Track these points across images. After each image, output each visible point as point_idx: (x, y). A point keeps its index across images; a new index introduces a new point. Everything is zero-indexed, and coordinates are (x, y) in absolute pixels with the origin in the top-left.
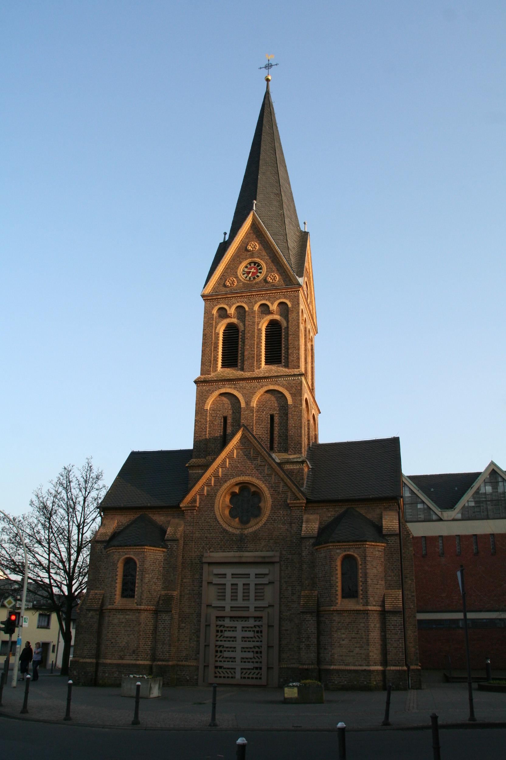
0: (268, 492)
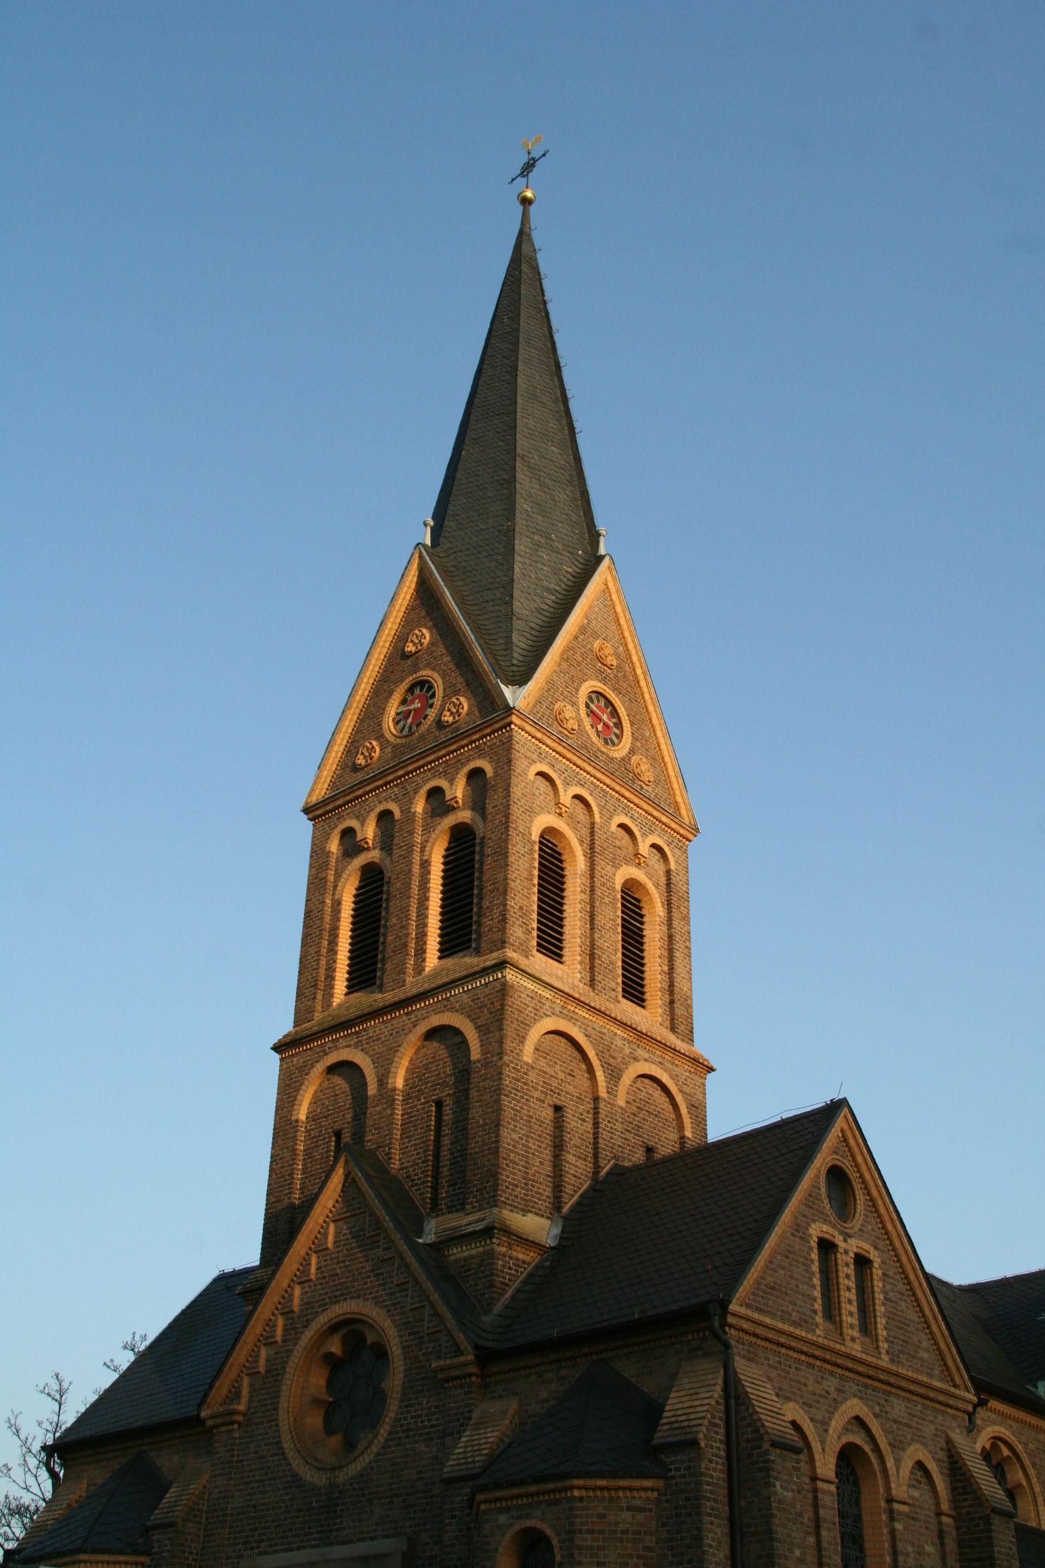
0: (397, 1340)
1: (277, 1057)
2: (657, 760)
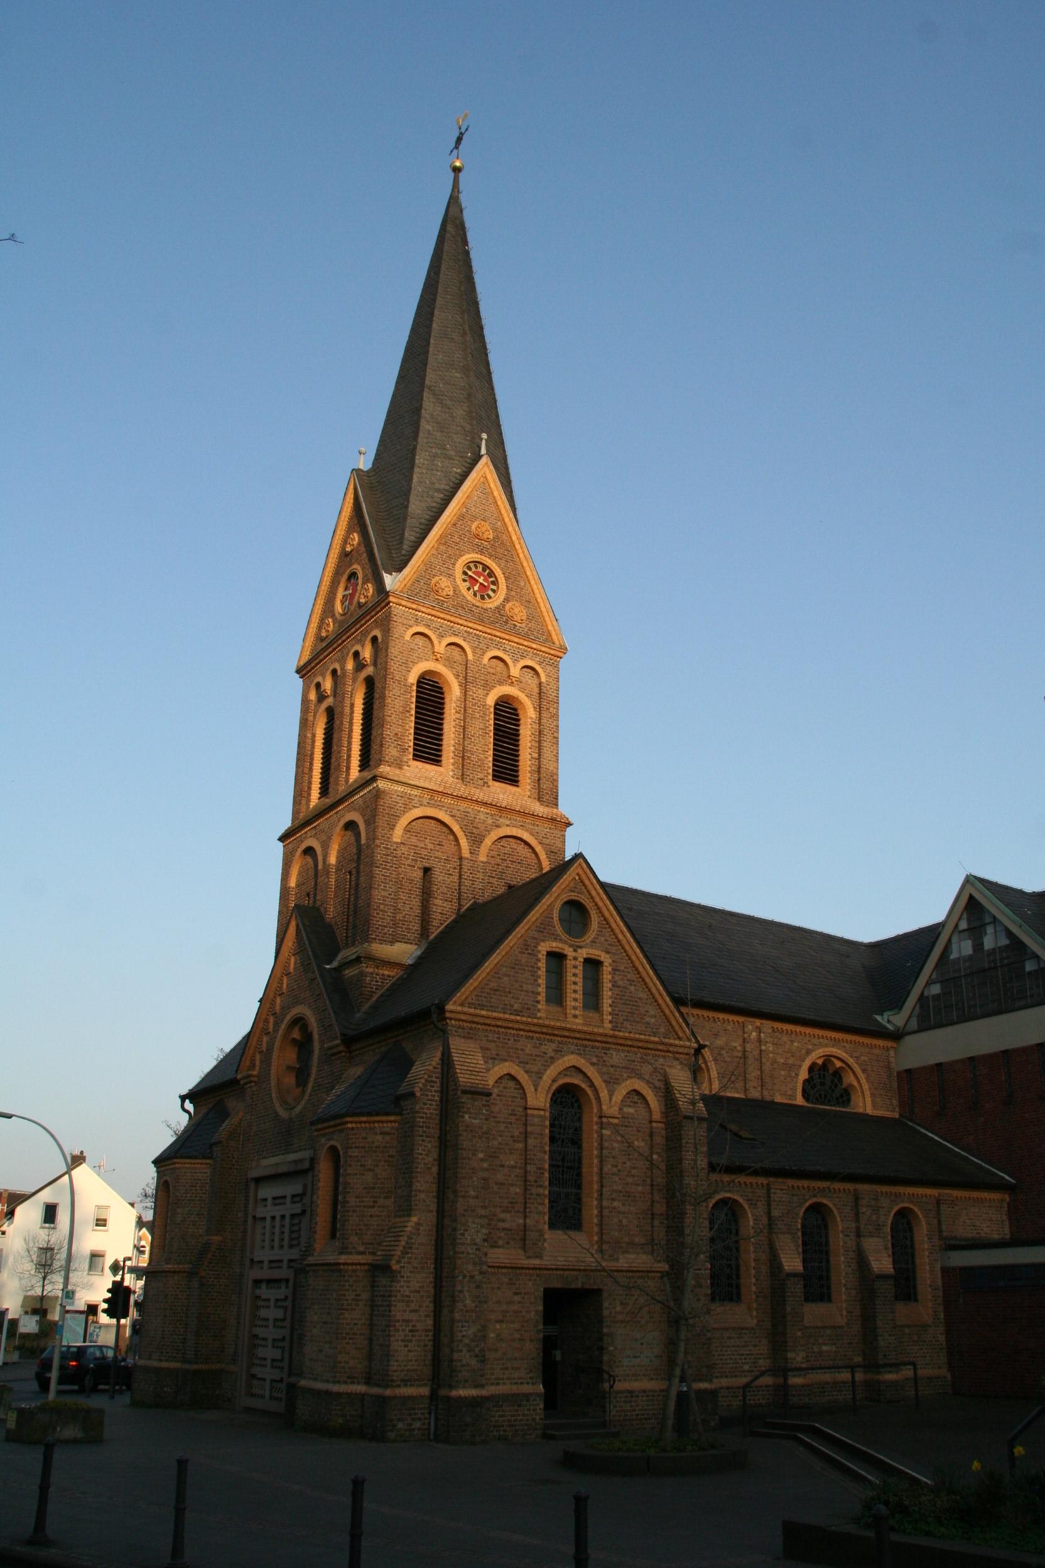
1: (281, 844)
2: (530, 603)
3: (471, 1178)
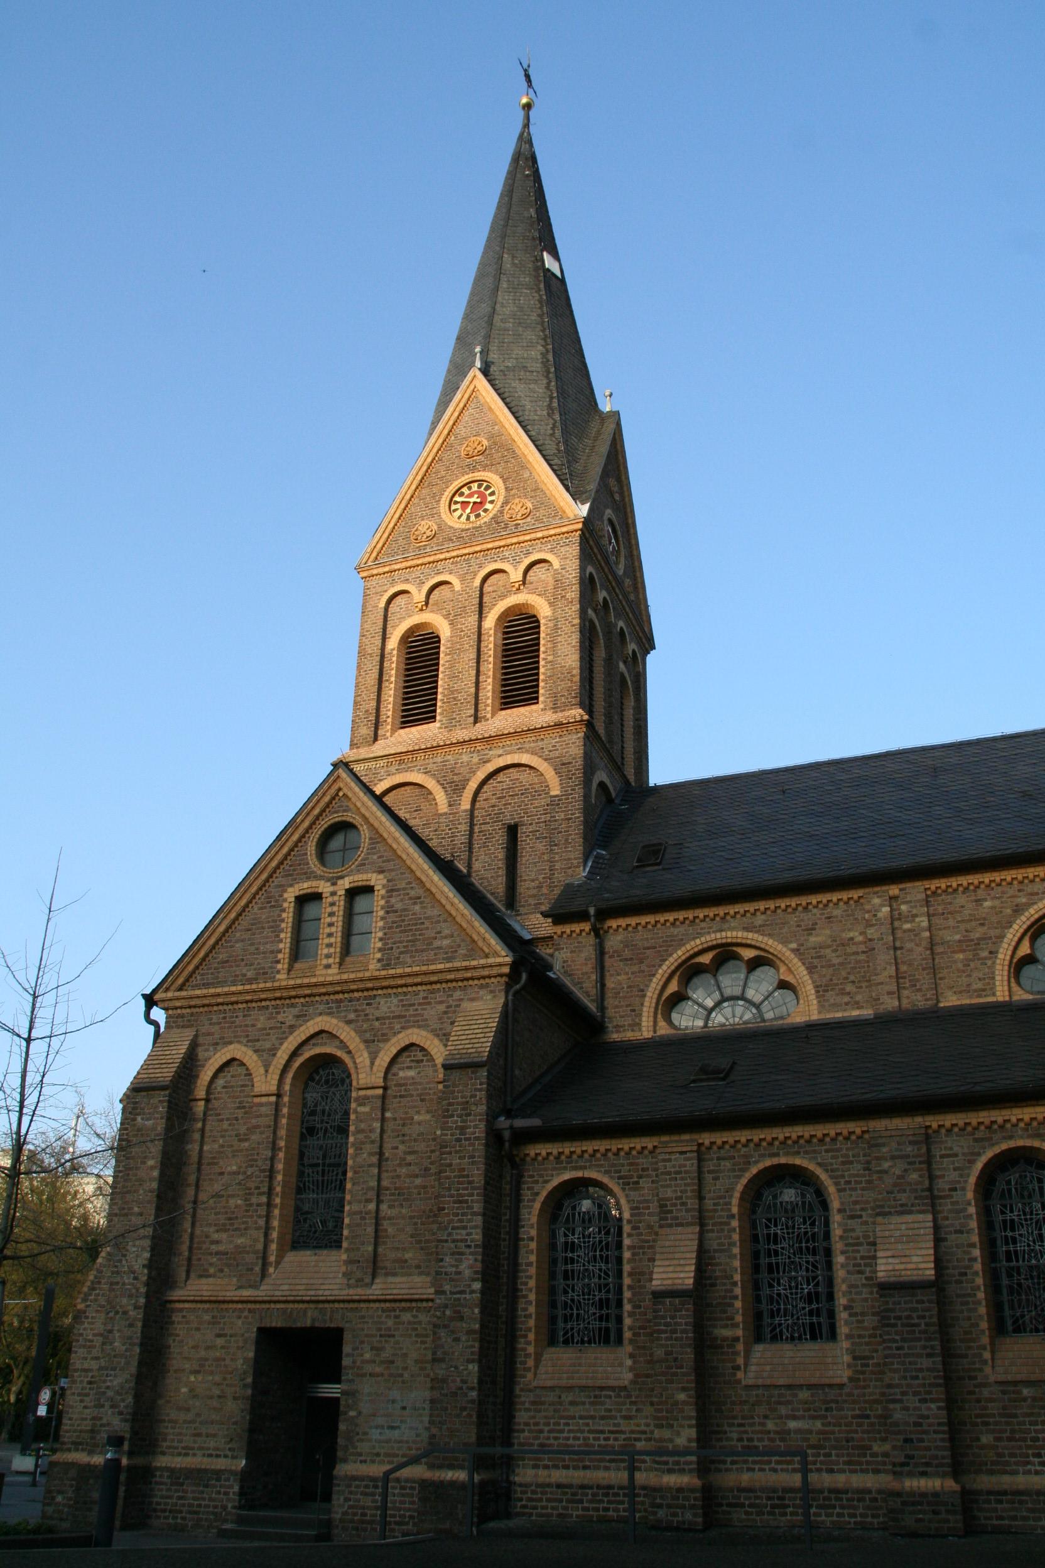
3: (136, 1191)
